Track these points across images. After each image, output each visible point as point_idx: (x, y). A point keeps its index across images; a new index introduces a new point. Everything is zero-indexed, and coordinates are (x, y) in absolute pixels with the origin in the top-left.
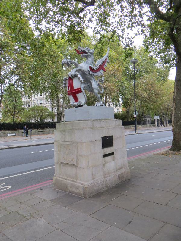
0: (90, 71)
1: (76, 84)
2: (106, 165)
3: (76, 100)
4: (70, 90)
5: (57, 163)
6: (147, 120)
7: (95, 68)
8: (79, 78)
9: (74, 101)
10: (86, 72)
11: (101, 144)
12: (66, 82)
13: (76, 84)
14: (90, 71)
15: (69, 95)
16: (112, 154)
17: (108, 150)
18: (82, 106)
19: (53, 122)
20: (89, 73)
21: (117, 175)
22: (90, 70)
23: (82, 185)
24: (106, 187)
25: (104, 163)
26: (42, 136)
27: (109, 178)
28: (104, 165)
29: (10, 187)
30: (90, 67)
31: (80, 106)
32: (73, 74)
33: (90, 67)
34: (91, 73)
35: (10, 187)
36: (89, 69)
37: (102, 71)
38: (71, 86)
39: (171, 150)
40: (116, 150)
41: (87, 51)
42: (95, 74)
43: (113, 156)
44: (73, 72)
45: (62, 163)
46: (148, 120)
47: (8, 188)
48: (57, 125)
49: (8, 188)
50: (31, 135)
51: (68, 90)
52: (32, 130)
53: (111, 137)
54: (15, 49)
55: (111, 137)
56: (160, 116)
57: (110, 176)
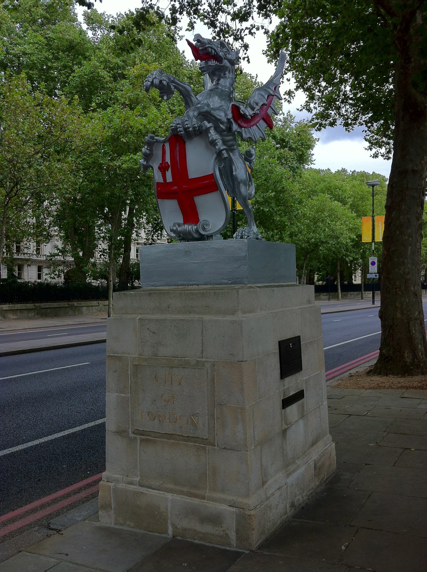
0: (232, 120)
2: (289, 433)
3: (190, 214)
4: (169, 178)
7: (249, 112)
8: (213, 143)
9: (181, 221)
10: (222, 123)
14: (232, 120)
16: (300, 395)
17: (293, 384)
18: (209, 237)
19: (40, 284)
22: (234, 117)
23: (234, 509)
24: (293, 505)
25: (285, 427)
26: (399, 379)
31: (202, 238)
32: (188, 124)
34: (235, 127)
36: (230, 116)
38: (179, 165)
39: (370, 372)
40: (307, 381)
43: (300, 402)
45: (137, 432)
53: (297, 340)
54: (343, 42)
55: (297, 340)
57: (298, 467)
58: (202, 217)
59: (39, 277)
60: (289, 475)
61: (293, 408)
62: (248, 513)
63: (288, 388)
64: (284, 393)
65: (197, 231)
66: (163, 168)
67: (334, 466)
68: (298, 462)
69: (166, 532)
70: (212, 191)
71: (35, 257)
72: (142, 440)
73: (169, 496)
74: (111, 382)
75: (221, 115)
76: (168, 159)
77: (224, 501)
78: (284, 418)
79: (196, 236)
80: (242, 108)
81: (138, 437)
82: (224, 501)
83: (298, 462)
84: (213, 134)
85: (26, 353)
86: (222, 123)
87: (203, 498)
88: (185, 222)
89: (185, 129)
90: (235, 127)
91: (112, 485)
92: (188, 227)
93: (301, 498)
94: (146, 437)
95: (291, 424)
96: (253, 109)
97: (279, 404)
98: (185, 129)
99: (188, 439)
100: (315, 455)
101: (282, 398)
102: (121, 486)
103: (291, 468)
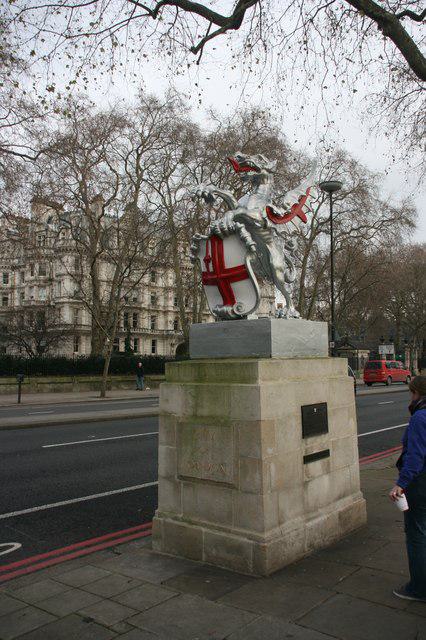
1: (232, 256)
2: (310, 484)
4: (211, 269)
5: (168, 478)
6: (360, 356)
7: (281, 212)
9: (222, 303)
10: (258, 222)
11: (300, 427)
12: (198, 246)
13: (232, 256)
15: (206, 282)
16: (325, 454)
17: (316, 444)
20: (265, 226)
21: (335, 513)
23: (252, 542)
24: (311, 546)
27: (316, 521)
28: (305, 484)
29: (17, 545)
30: (270, 211)
33: (270, 211)
34: (269, 224)
35: (17, 545)
36: (265, 214)
37: (296, 220)
38: (217, 258)
41: (259, 166)
42: (280, 228)
43: (325, 460)
44: (227, 220)
45: (181, 477)
46: (363, 358)
47: (12, 550)
48: (170, 371)
49: (12, 550)
50: (20, 394)
51: (204, 269)
52: (22, 379)
53: (323, 407)
55: (323, 407)
56: (396, 346)
57: (319, 515)
58: (238, 300)
59: (153, 350)
60: (308, 520)
61: (316, 466)
62: (262, 544)
63: (312, 447)
64: (306, 450)
65: (233, 312)
66: (207, 261)
67: (364, 519)
68: (320, 510)
69: (201, 559)
70: (243, 279)
71: (149, 332)
72: (185, 485)
73: (204, 530)
74: (162, 437)
75: (256, 215)
76: (210, 254)
77: (245, 535)
78: (307, 473)
79: (232, 316)
80: (275, 208)
81: (182, 482)
82: (245, 535)
83: (320, 510)
84: (245, 233)
85: (62, 373)
86: (258, 222)
87: (230, 532)
88: (225, 304)
89: (222, 230)
90: (269, 224)
91: (161, 519)
92: (227, 309)
93: (318, 542)
94: (188, 480)
95: (313, 478)
96: (285, 208)
97: (301, 460)
98: (222, 230)
99: (219, 484)
100: (340, 506)
101: (304, 454)
102: (170, 520)
103: (311, 515)
